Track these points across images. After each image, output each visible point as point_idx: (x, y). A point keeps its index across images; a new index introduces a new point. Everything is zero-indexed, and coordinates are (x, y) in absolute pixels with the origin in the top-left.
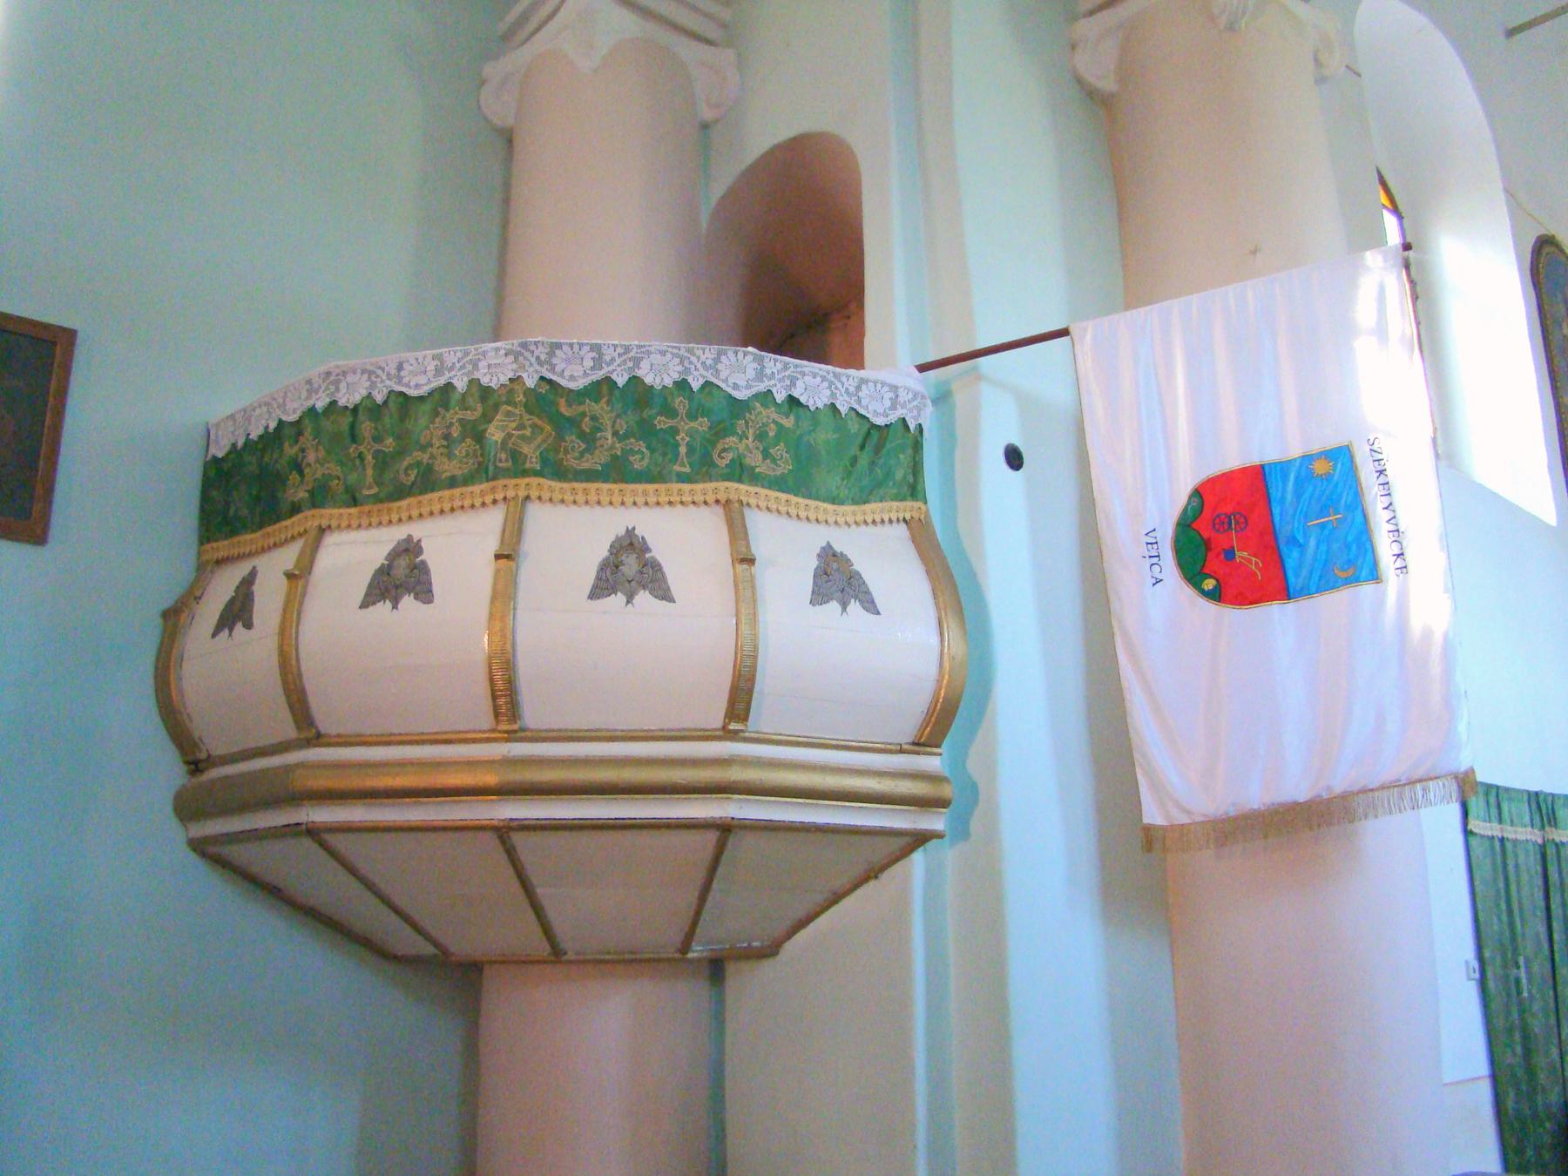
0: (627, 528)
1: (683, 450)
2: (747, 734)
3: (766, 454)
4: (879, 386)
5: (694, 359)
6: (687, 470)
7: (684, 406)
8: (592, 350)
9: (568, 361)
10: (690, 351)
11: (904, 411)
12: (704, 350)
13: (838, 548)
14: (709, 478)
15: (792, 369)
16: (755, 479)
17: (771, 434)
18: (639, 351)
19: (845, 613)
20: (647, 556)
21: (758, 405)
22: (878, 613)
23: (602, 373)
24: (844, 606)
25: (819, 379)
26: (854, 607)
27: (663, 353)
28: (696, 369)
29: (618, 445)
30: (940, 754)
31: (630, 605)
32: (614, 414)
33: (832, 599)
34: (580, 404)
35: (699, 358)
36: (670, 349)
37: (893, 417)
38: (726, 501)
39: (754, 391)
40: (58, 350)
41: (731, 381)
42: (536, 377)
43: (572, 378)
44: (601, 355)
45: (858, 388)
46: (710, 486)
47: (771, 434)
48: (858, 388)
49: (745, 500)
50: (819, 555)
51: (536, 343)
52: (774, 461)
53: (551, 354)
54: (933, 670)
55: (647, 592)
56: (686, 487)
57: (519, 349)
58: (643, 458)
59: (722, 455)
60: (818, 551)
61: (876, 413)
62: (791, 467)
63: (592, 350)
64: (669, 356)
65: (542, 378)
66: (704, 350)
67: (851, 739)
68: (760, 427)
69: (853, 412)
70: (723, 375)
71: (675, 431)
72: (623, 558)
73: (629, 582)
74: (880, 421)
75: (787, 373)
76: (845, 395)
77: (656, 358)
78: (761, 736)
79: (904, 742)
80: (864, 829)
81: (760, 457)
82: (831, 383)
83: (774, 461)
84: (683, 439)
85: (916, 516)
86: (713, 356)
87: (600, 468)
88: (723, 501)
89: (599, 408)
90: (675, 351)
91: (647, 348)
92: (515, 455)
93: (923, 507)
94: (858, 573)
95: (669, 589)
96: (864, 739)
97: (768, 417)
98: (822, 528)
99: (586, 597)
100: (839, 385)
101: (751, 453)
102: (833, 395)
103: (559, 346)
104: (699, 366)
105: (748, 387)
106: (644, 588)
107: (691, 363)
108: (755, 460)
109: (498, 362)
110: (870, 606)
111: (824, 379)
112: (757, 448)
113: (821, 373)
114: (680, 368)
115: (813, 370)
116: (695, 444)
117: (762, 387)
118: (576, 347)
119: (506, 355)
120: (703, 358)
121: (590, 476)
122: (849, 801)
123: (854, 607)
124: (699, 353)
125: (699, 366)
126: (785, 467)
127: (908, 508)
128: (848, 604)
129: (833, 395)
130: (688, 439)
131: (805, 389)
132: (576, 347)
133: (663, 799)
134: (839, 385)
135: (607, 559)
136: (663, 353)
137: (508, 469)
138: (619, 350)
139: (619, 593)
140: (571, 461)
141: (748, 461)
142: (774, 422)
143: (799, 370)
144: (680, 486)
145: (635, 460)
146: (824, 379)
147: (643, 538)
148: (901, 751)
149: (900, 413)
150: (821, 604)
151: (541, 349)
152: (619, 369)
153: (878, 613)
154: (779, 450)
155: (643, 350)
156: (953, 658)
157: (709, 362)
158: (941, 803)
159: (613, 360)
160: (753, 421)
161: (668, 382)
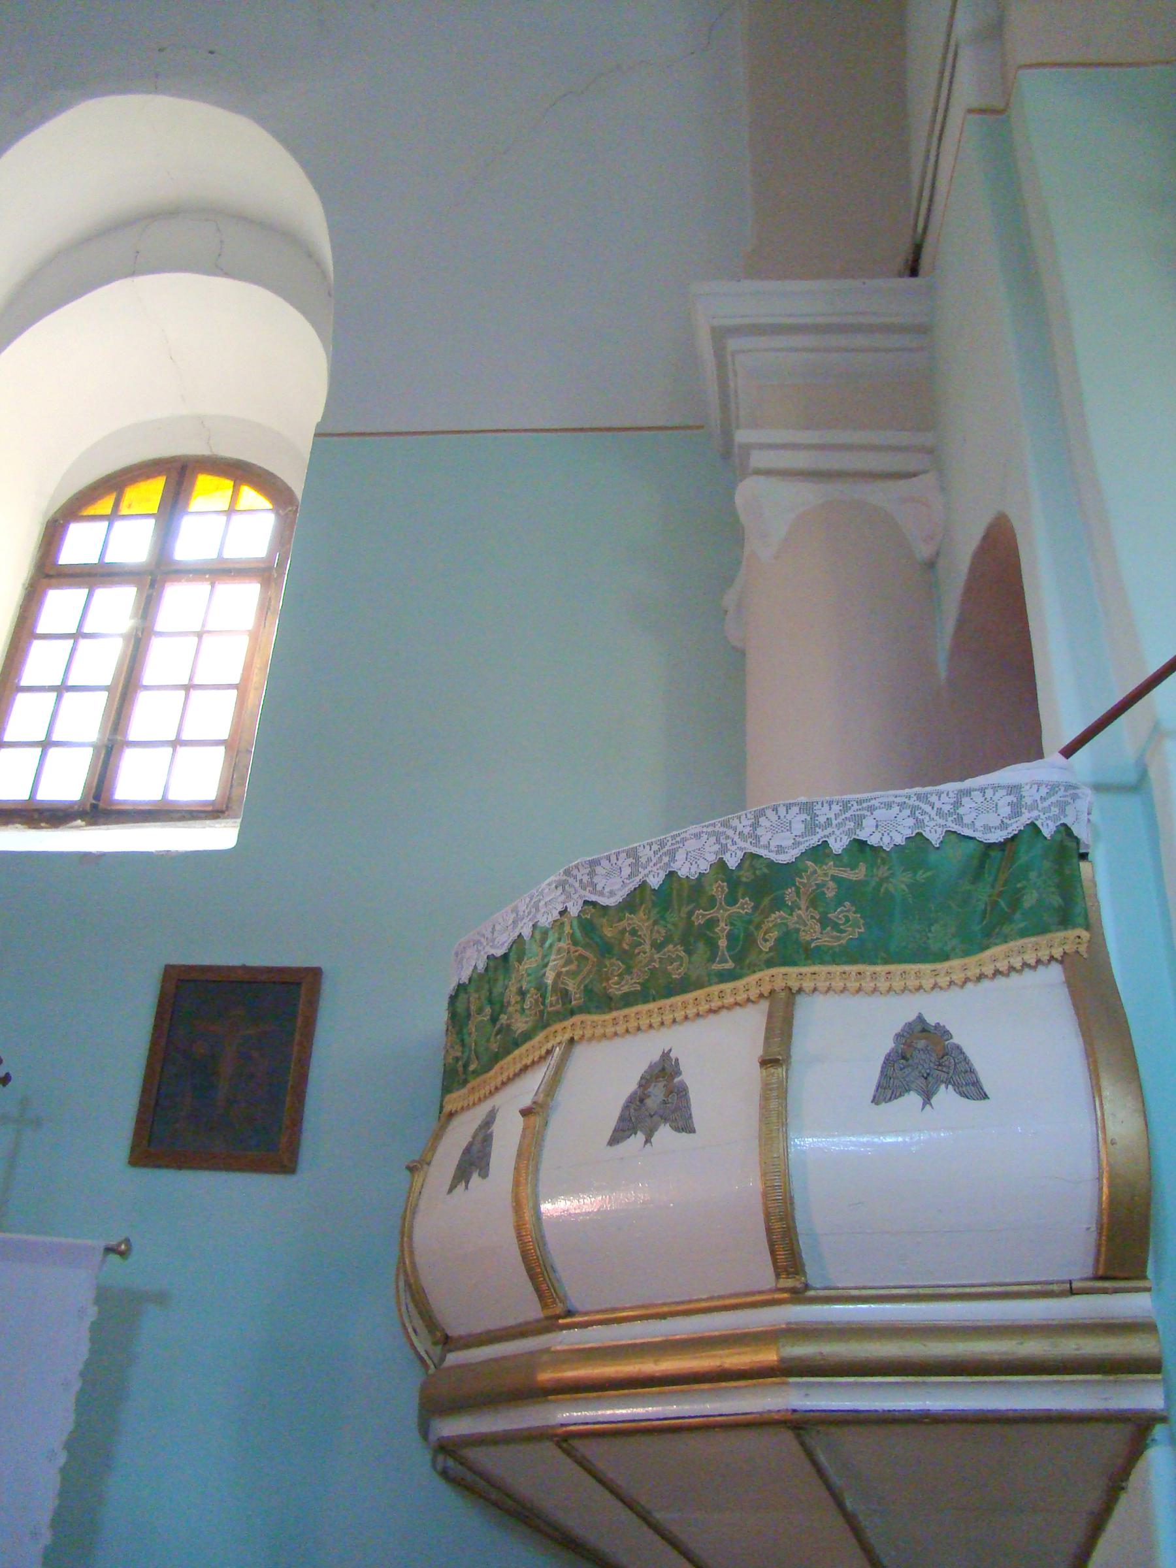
0: (664, 1050)
1: (723, 943)
2: (811, 1293)
3: (824, 921)
4: (782, 811)
5: (730, 832)
6: (730, 965)
7: (723, 891)
8: (628, 856)
9: (608, 875)
10: (725, 824)
11: (1035, 813)
12: (739, 818)
13: (931, 1020)
14: (753, 968)
15: (856, 807)
16: (812, 954)
17: (830, 894)
18: (674, 842)
19: (928, 1107)
20: (676, 1080)
21: (809, 863)
22: (985, 1097)
23: (638, 879)
24: (927, 1097)
25: (896, 809)
26: (945, 1096)
27: (697, 836)
28: (734, 843)
29: (656, 956)
30: (1148, 1290)
31: (649, 1144)
32: (651, 922)
33: (908, 1091)
34: (620, 920)
35: (735, 829)
36: (705, 830)
37: (1015, 826)
38: (770, 993)
39: (803, 848)
40: (304, 988)
41: (773, 844)
42: (581, 903)
43: (612, 893)
44: (637, 858)
45: (957, 804)
46: (752, 979)
47: (830, 894)
48: (957, 804)
49: (795, 986)
50: (898, 1036)
51: (577, 867)
52: (836, 926)
53: (592, 874)
54: (1087, 1167)
55: (668, 1125)
56: (727, 987)
57: (565, 878)
58: (681, 965)
59: (766, 937)
60: (898, 1028)
61: (988, 829)
62: (862, 930)
63: (628, 856)
64: (705, 837)
65: (586, 902)
66: (739, 818)
67: (985, 1281)
68: (813, 891)
69: (953, 837)
70: (967, 820)
71: (712, 923)
72: (650, 1090)
73: (651, 1116)
74: (997, 837)
75: (848, 815)
76: (937, 818)
77: (692, 845)
78: (833, 1293)
79: (1078, 1277)
80: (1011, 1414)
81: (818, 927)
82: (914, 809)
83: (836, 926)
84: (723, 930)
85: (1068, 948)
86: (750, 822)
87: (639, 988)
88: (766, 994)
89: (640, 920)
90: (710, 829)
91: (682, 836)
92: (565, 995)
93: (1085, 935)
94: (958, 1048)
95: (690, 1117)
96: (884, 1284)
97: (826, 875)
98: (907, 998)
99: (606, 1143)
100: (927, 808)
101: (806, 925)
102: (919, 823)
103: (594, 863)
104: (736, 838)
105: (796, 844)
106: (666, 1120)
107: (728, 837)
108: (813, 933)
109: (551, 898)
110: (972, 1088)
111: (902, 806)
112: (813, 917)
113: (898, 800)
114: (717, 847)
115: (885, 800)
116: (736, 931)
117: (814, 840)
118: (613, 858)
119: (556, 887)
120: (938, 805)
121: (628, 1000)
122: (813, 1376)
123: (945, 1096)
124: (735, 823)
125: (736, 838)
126: (853, 933)
127: (1062, 940)
128: (934, 1093)
129: (919, 823)
130: (728, 928)
131: (877, 826)
132: (613, 858)
133: (682, 1391)
134: (927, 808)
135: (635, 1093)
136: (697, 836)
137: (558, 1012)
138: (655, 847)
139: (639, 1132)
140: (616, 990)
141: (805, 937)
142: (834, 878)
143: (865, 805)
144: (722, 986)
145: (673, 969)
146: (902, 806)
147: (677, 1060)
148: (1072, 1292)
149: (1025, 818)
150: (890, 1100)
151: (583, 871)
152: (655, 869)
153: (985, 1097)
154: (844, 913)
155: (678, 839)
156: (1113, 1143)
157: (946, 808)
158: (1150, 1366)
159: (649, 860)
160: (804, 885)
161: (704, 867)
